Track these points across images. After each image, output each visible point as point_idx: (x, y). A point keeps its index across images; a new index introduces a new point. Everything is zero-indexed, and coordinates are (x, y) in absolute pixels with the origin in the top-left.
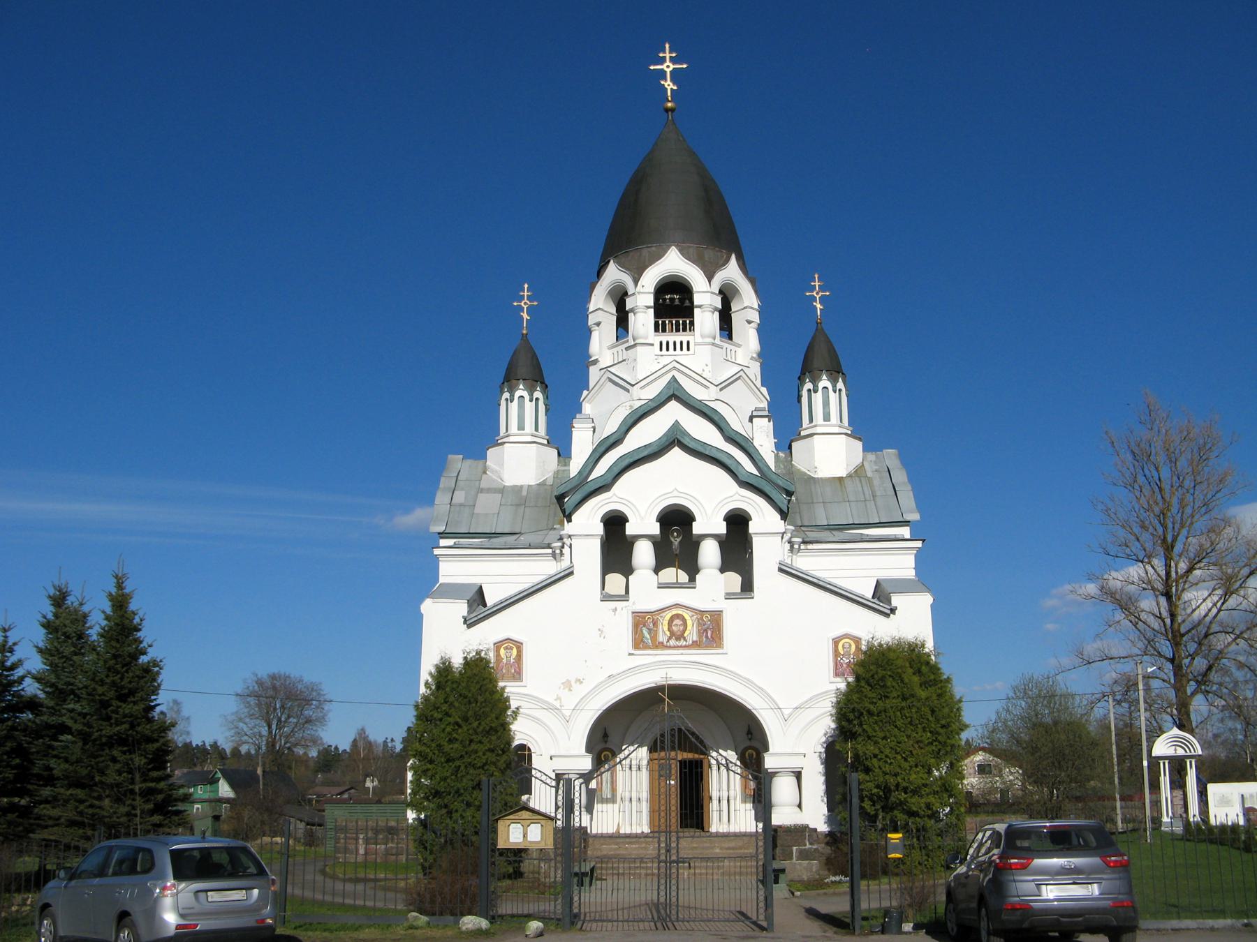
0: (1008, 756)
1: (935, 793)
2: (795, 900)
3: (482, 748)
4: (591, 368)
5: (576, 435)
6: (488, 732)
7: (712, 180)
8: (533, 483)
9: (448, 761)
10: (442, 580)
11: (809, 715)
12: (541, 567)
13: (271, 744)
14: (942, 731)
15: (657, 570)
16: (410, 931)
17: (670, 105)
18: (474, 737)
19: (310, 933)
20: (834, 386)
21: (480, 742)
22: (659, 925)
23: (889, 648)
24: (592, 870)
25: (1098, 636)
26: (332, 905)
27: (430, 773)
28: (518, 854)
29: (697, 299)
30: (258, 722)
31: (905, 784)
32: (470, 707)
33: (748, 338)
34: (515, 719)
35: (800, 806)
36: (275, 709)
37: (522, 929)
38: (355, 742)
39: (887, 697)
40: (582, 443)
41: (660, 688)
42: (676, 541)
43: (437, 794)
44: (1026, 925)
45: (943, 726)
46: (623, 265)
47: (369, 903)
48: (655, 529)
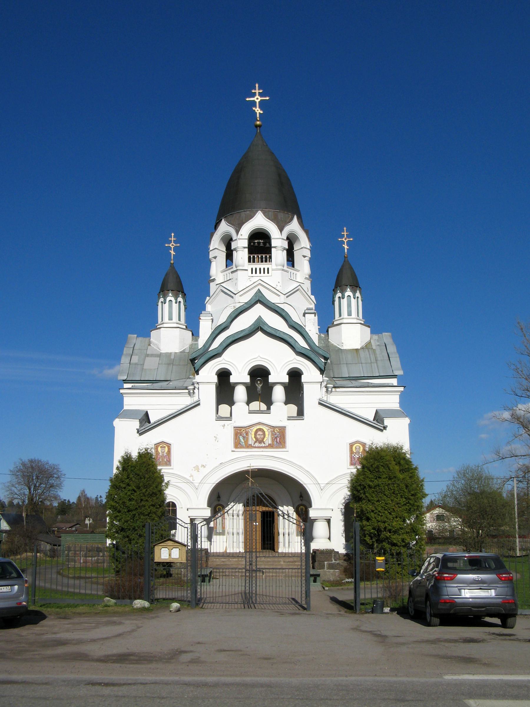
0: (455, 511)
1: (407, 533)
2: (325, 592)
3: (148, 504)
4: (212, 284)
5: (202, 323)
6: (151, 495)
7: (284, 171)
9: (129, 511)
10: (126, 408)
11: (335, 487)
12: (182, 400)
13: (31, 499)
14: (412, 498)
15: (248, 403)
16: (106, 608)
17: (258, 123)
18: (143, 498)
19: (49, 609)
20: (354, 295)
21: (147, 501)
22: (246, 605)
23: (382, 450)
24: (211, 573)
25: (508, 443)
26: (62, 592)
27: (118, 518)
28: (168, 565)
30: (23, 487)
31: (390, 528)
32: (141, 478)
33: (303, 266)
34: (167, 487)
35: (329, 539)
36: (33, 479)
37: (168, 607)
38: (79, 498)
39: (380, 478)
40: (206, 328)
41: (246, 472)
42: (259, 386)
43: (122, 530)
44: (452, 612)
45: (412, 495)
46: (230, 222)
47: (83, 591)
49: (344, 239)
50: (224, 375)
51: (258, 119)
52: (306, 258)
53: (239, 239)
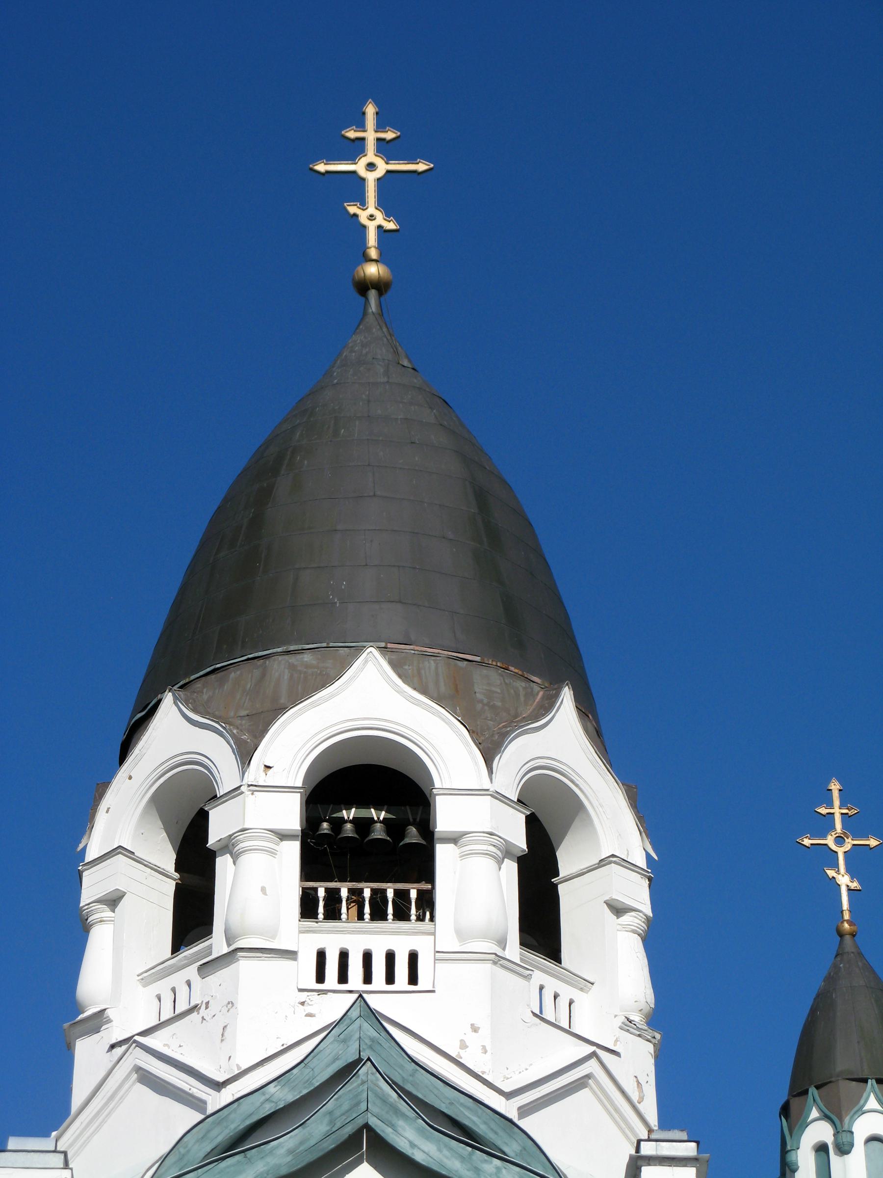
17: (372, 270)
29: (447, 815)
46: (207, 711)
49: (830, 841)
51: (373, 253)
52: (627, 919)
53: (255, 788)
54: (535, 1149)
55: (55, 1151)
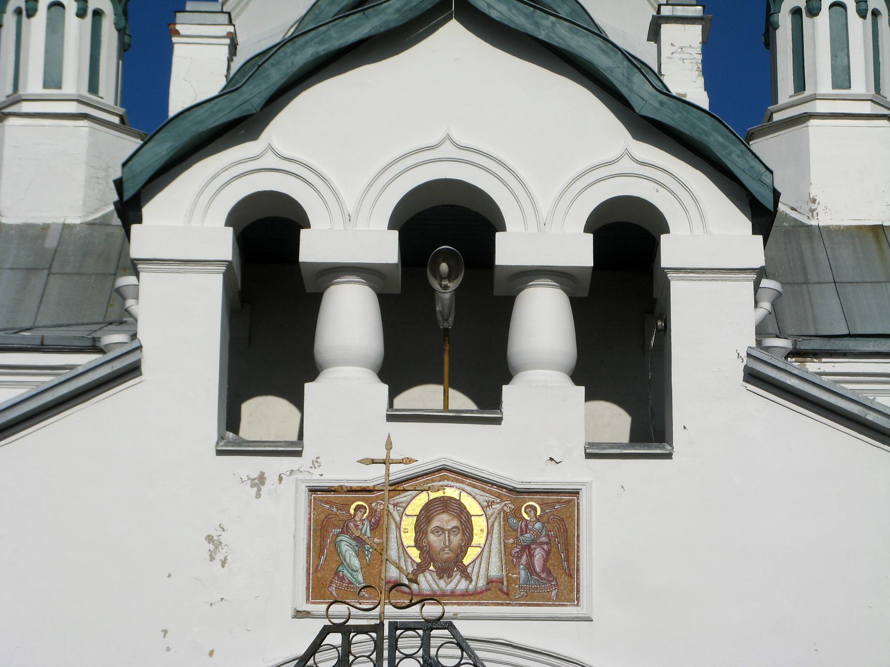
8: (75, 219)
42: (445, 290)
48: (386, 249)
50: (267, 235)
54: (581, 11)
55: (222, 12)
